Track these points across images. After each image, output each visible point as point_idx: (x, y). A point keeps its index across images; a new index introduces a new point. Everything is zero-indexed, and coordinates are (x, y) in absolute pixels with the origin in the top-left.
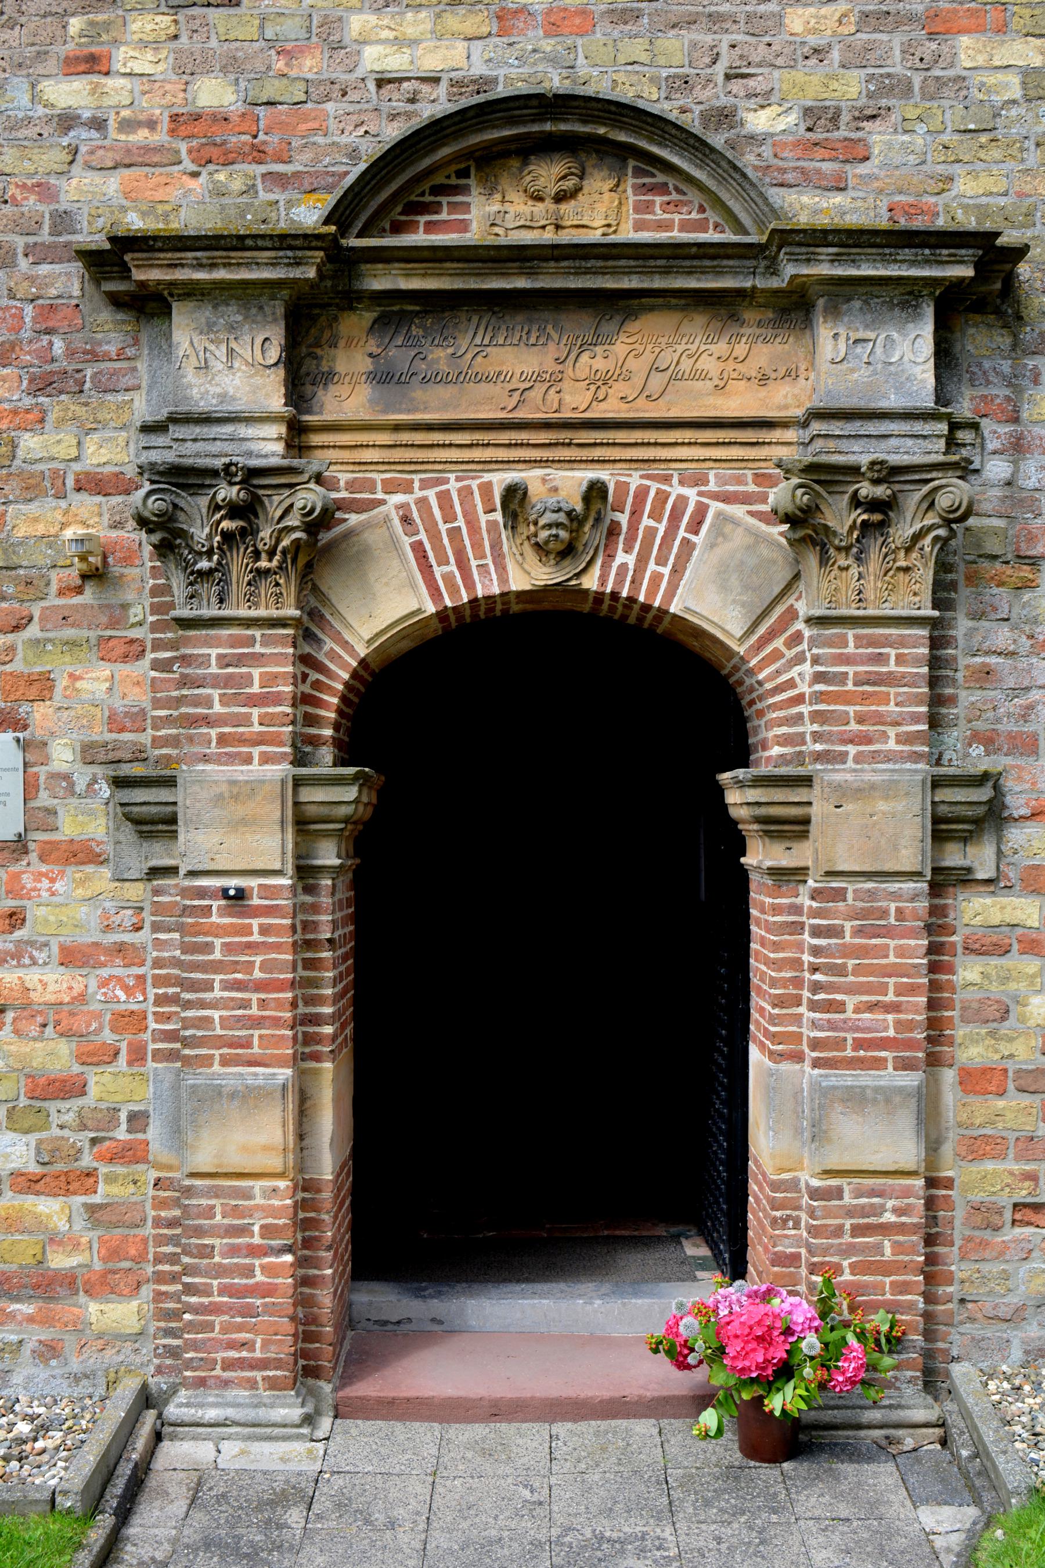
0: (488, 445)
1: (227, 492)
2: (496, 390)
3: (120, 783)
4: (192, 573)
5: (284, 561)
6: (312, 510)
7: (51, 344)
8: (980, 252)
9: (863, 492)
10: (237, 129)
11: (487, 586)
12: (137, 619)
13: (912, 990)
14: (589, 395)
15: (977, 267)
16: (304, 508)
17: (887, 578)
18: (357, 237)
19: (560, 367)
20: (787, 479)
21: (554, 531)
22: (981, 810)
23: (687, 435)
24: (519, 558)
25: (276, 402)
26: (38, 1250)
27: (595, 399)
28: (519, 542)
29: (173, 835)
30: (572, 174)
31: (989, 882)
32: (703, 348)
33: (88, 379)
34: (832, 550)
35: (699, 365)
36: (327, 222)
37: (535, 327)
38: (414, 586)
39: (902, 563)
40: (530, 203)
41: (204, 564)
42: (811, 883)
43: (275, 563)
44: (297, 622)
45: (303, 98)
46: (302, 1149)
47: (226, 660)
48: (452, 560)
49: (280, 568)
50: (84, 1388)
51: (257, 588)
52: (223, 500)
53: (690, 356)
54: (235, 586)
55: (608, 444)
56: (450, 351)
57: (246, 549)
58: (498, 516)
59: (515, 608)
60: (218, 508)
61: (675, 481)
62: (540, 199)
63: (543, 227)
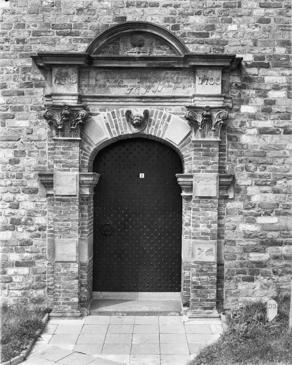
2: (126, 89)
3: (40, 175)
4: (57, 129)
5: (77, 127)
6: (84, 115)
8: (231, 60)
9: (204, 113)
13: (214, 222)
16: (81, 115)
18: (94, 54)
22: (230, 183)
29: (53, 187)
31: (232, 199)
32: (171, 80)
36: (86, 51)
41: (60, 127)
43: (75, 127)
48: (115, 127)
49: (76, 128)
50: (10, 63)
56: (114, 80)
58: (125, 117)
59: (130, 137)
60: (62, 115)
61: (164, 110)
63: (135, 52)
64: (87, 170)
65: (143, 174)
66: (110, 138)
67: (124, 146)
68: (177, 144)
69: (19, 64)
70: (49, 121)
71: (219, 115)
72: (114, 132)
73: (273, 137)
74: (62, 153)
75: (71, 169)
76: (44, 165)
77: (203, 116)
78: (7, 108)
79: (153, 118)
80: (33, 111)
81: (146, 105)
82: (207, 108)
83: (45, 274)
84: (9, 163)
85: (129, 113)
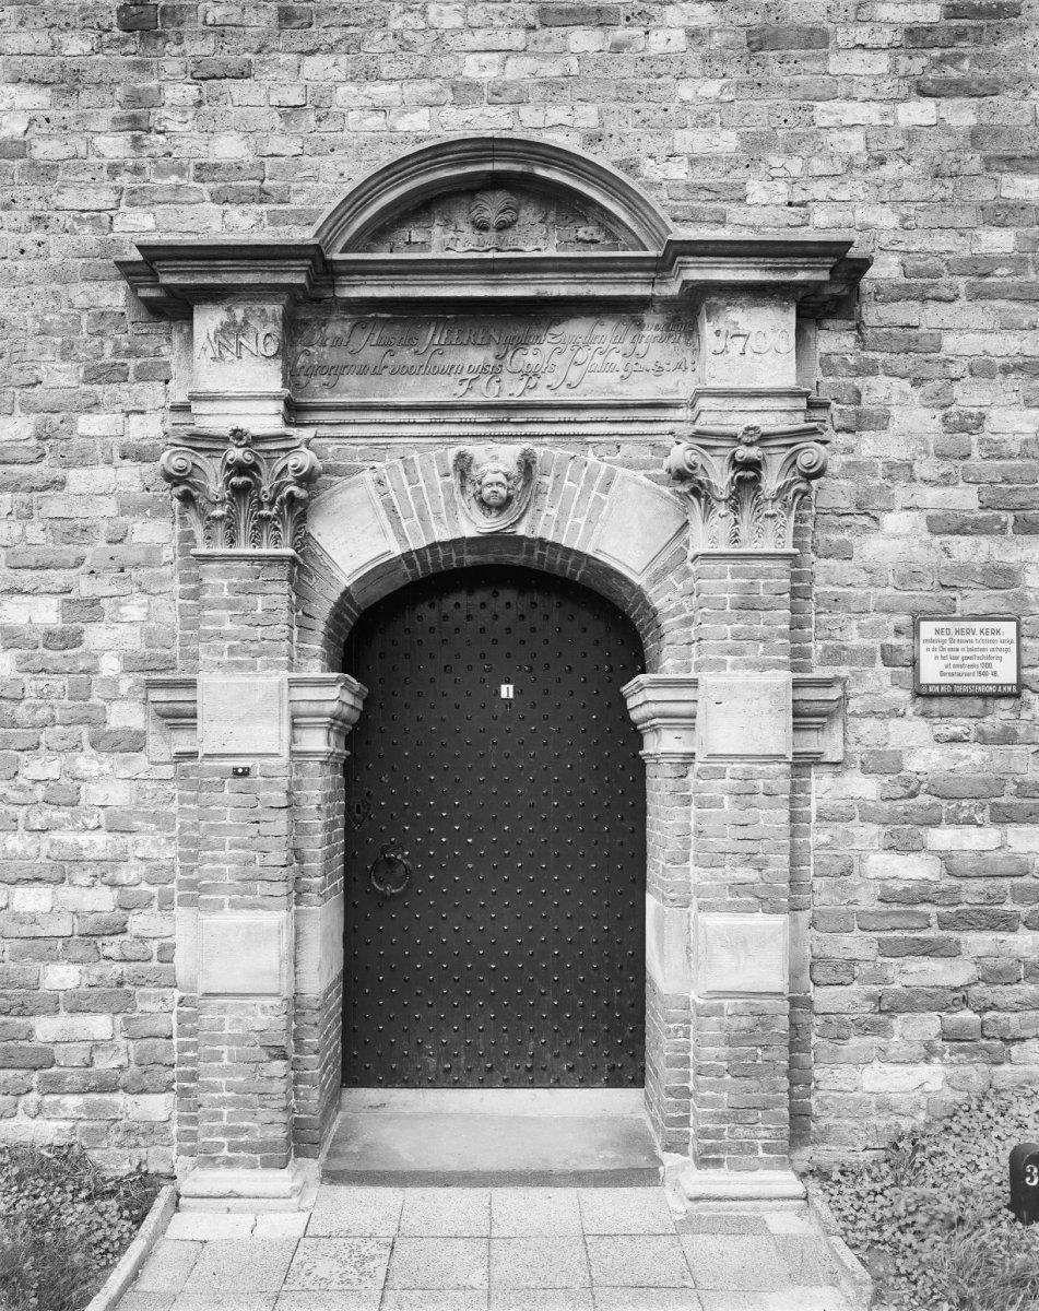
0: (444, 422)
1: (236, 453)
4: (209, 519)
7: (102, 343)
10: (247, 176)
11: (443, 534)
12: (168, 559)
14: (523, 383)
15: (832, 271)
16: (294, 466)
17: (758, 523)
18: (341, 252)
19: (500, 362)
20: (678, 443)
21: (495, 488)
23: (599, 414)
24: (467, 510)
25: (275, 385)
26: (86, 1054)
27: (527, 387)
28: (467, 498)
30: (510, 208)
33: (131, 372)
34: (713, 501)
35: (609, 360)
37: (481, 331)
38: (384, 533)
39: (770, 512)
40: (477, 232)
41: (218, 512)
42: (697, 765)
43: (274, 511)
44: (293, 560)
45: (300, 151)
46: (296, 974)
47: (236, 588)
48: (415, 515)
49: (278, 515)
51: (261, 531)
52: (232, 460)
53: (601, 353)
54: (242, 531)
55: (537, 422)
57: (251, 500)
62: (485, 229)
64: (318, 668)
65: (511, 687)
66: (398, 551)
67: (432, 606)
68: (639, 571)
69: (81, 301)
70: (182, 488)
71: (792, 460)
72: (219, 1116)
73: (978, 545)
74: (231, 606)
75: (259, 660)
76: (168, 652)
77: (736, 464)
78: (40, 452)
79: (549, 480)
80: (127, 461)
81: (526, 435)
82: (752, 432)
83: (170, 1037)
84: (45, 646)
85: (463, 466)
